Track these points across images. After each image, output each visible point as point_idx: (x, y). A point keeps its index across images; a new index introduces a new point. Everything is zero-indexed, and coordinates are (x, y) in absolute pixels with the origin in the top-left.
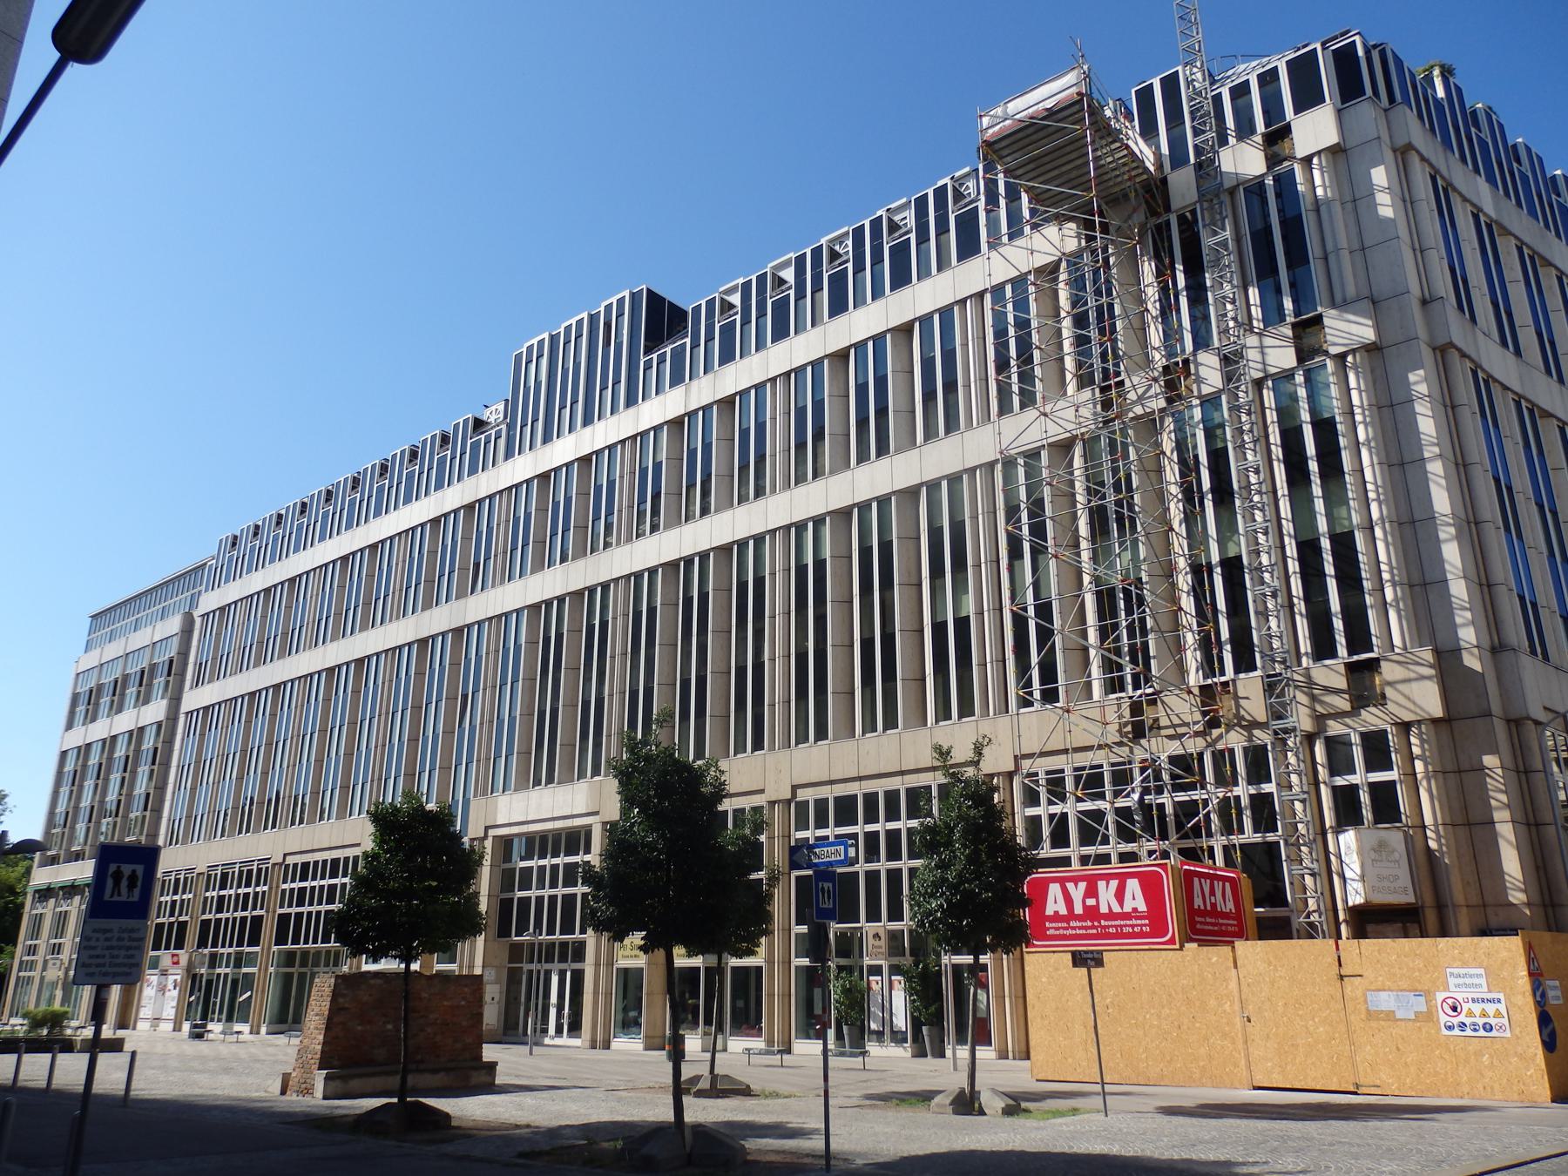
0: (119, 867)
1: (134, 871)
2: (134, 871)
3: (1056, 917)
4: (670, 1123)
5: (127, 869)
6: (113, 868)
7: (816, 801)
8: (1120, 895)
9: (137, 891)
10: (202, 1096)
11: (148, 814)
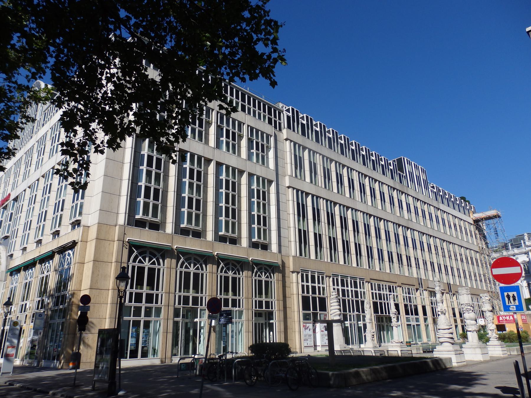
0: (508, 293)
1: (513, 295)
2: (513, 295)
3: (501, 320)
4: (327, 356)
5: (511, 294)
6: (506, 294)
7: (136, 357)
8: (510, 318)
9: (517, 301)
10: (321, 355)
11: (180, 319)
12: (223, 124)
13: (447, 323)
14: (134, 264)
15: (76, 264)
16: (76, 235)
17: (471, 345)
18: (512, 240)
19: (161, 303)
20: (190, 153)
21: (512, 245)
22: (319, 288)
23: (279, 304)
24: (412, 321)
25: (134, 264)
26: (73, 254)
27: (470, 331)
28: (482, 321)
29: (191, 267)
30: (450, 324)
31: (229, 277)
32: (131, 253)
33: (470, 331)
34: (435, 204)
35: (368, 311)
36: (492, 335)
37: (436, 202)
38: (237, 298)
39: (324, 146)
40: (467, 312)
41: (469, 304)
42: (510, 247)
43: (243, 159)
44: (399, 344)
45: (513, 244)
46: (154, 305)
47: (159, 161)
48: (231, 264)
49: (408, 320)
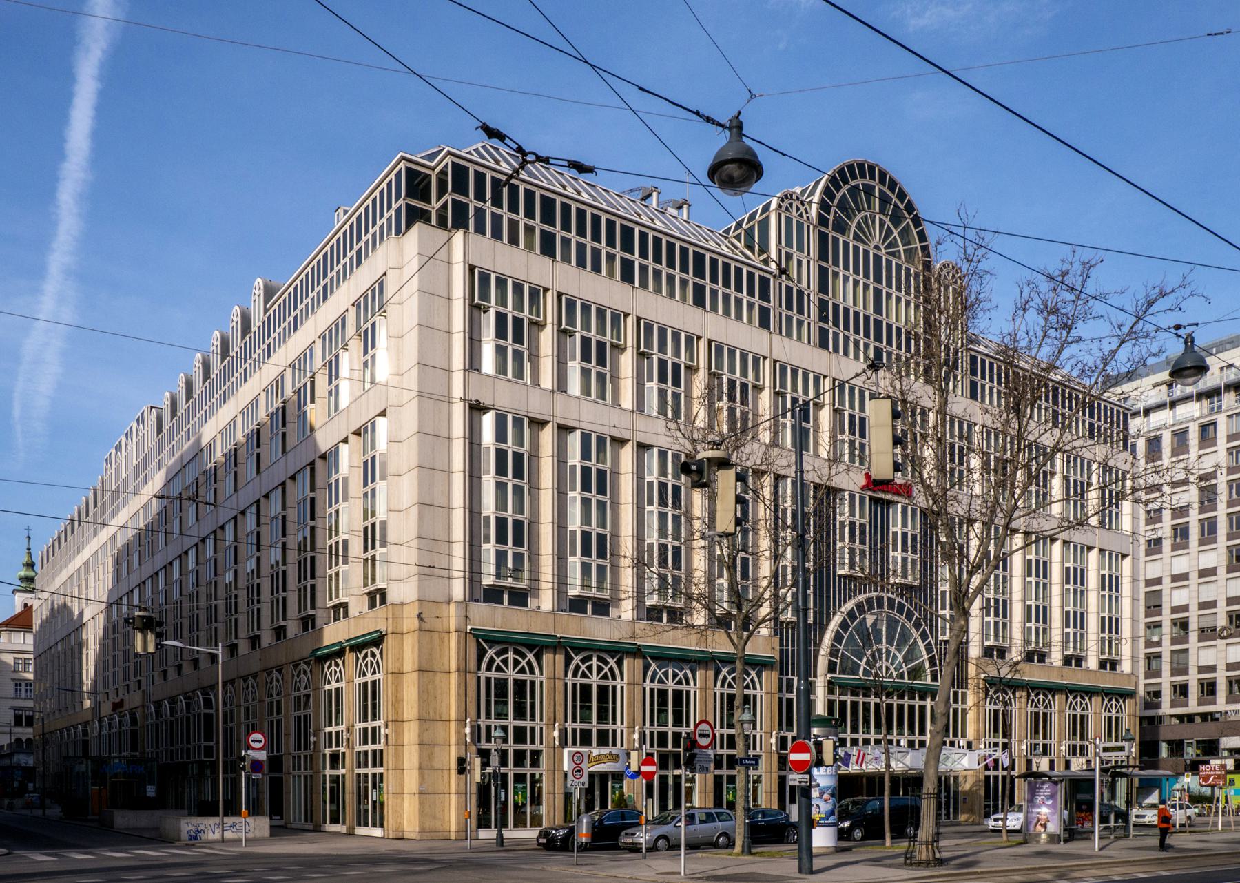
12: (488, 300)
14: (489, 674)
15: (390, 676)
16: (374, 621)
19: (541, 743)
20: (582, 433)
25: (489, 674)
26: (381, 653)
29: (507, 667)
31: (667, 690)
32: (481, 653)
38: (528, 724)
39: (806, 341)
43: (544, 389)
46: (528, 747)
47: (676, 489)
48: (595, 659)
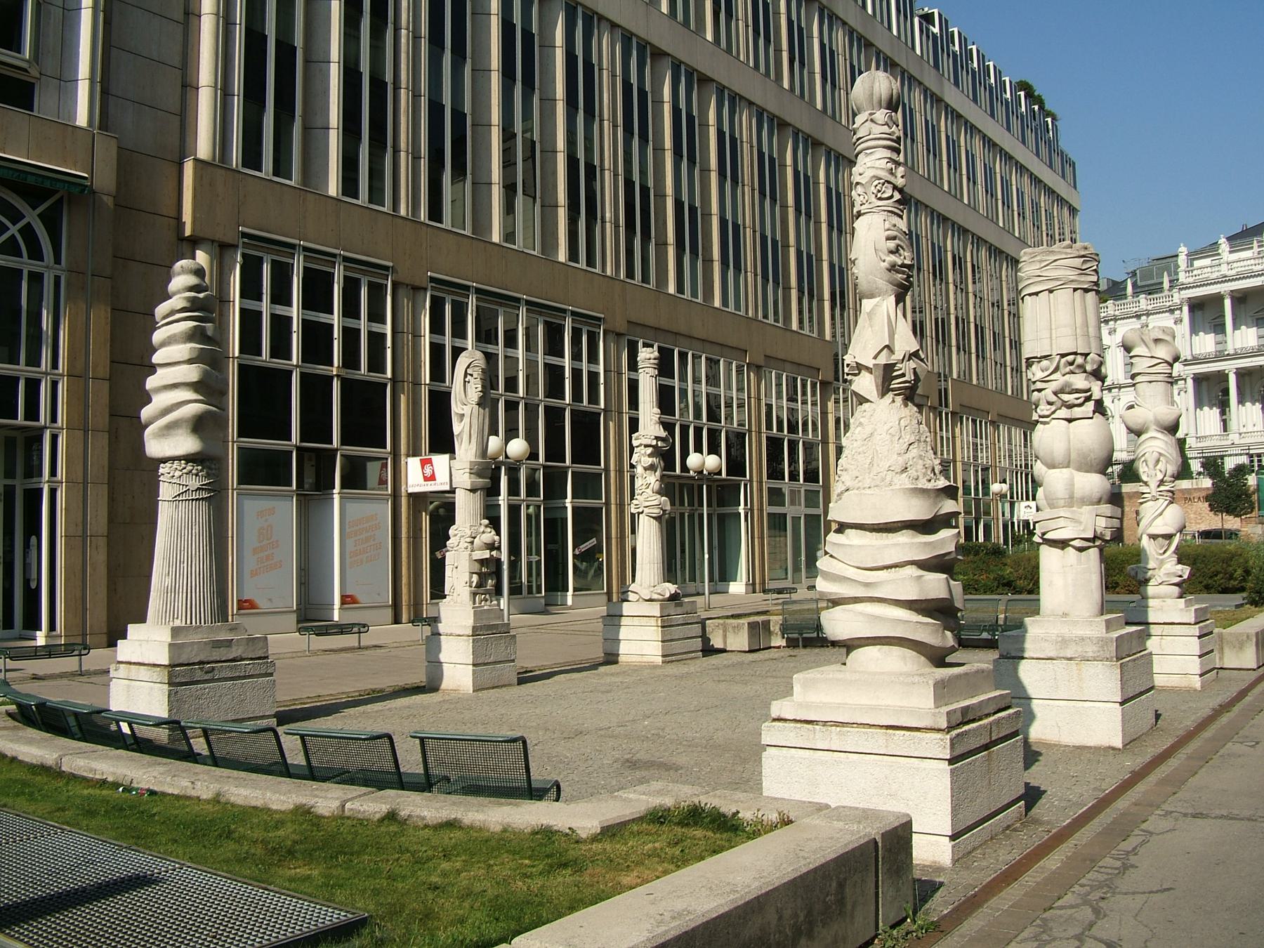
13: (917, 469)
17: (1064, 642)
18: (1138, 272)
21: (1134, 285)
22: (351, 336)
23: (79, 400)
24: (793, 503)
27: (1062, 544)
28: (1029, 510)
30: (942, 483)
33: (1062, 544)
34: (930, 79)
35: (466, 420)
36: (1162, 562)
37: (933, 71)
40: (1064, 413)
41: (1080, 360)
42: (1129, 289)
44: (904, 537)
45: (1139, 283)
49: (776, 496)
